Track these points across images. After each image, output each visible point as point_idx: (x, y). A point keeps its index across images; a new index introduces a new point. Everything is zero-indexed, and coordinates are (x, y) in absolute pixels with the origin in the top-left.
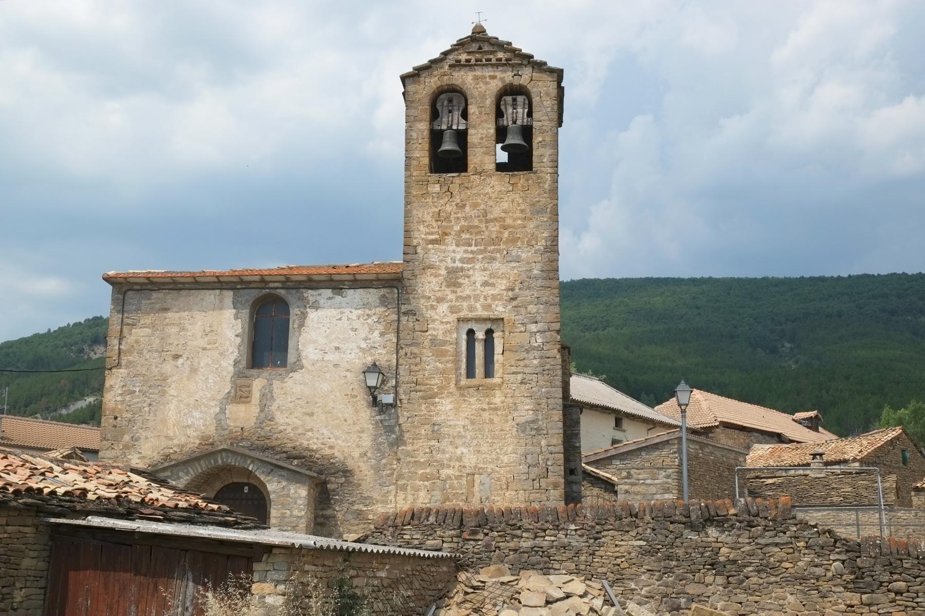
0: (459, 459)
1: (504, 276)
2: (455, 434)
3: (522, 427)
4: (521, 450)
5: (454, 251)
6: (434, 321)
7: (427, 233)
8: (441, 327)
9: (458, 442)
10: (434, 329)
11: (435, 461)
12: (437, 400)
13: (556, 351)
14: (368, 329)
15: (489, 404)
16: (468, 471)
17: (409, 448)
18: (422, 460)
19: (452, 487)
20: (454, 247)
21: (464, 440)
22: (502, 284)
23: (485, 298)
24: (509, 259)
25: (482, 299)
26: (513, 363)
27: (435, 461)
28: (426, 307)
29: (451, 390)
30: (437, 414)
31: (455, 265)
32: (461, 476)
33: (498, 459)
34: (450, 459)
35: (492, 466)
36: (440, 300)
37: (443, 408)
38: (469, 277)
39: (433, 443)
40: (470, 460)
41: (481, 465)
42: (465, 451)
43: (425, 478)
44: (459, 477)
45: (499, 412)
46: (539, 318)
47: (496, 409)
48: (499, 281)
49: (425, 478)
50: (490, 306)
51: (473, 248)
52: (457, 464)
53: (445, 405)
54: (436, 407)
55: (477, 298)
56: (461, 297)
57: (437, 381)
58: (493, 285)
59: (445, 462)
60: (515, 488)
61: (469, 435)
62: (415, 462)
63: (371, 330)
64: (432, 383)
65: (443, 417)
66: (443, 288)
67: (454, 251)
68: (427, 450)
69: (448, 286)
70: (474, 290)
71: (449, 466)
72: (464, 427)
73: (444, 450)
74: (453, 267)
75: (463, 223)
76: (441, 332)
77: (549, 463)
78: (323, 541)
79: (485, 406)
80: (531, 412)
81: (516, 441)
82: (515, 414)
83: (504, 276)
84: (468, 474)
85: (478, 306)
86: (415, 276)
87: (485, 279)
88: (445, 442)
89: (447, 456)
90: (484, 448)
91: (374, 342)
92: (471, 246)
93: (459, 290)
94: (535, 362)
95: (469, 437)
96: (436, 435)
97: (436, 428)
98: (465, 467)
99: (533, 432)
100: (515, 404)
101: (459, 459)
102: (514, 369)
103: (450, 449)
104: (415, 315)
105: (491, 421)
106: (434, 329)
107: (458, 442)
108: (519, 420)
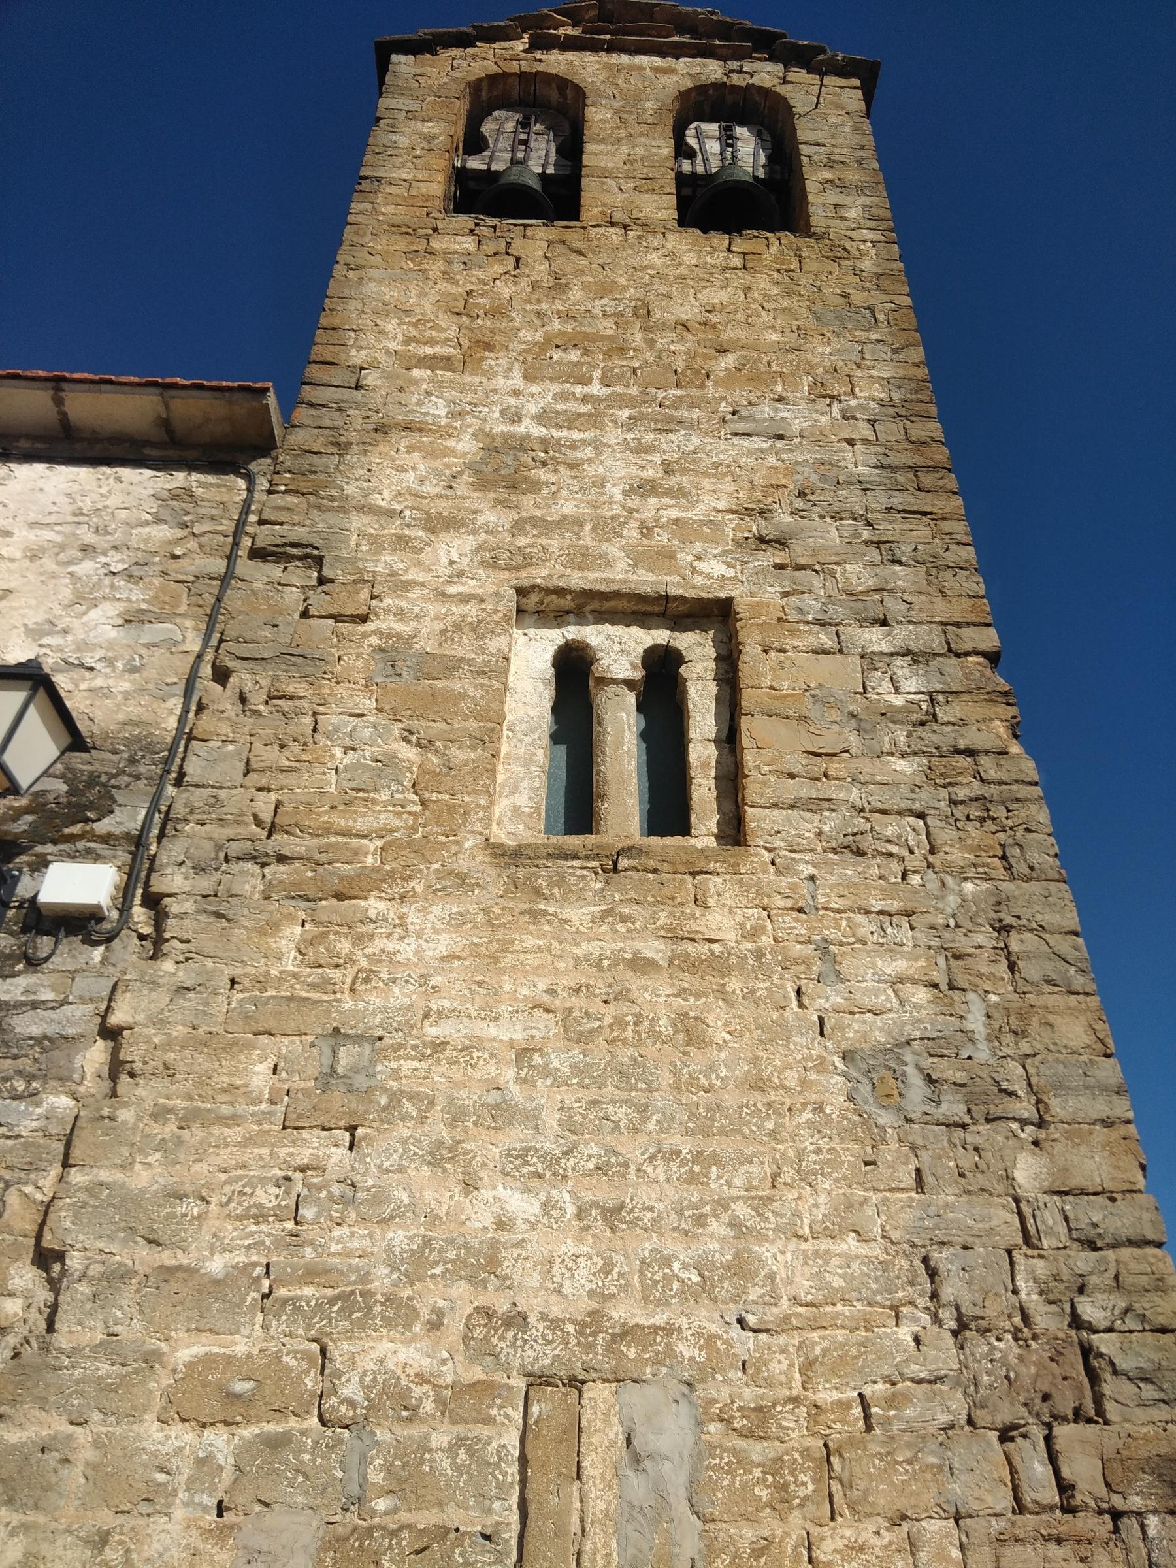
0: (483, 1264)
1: (720, 470)
2: (468, 1098)
3: (875, 1071)
4: (904, 1212)
5: (516, 393)
6: (407, 586)
7: (408, 340)
8: (435, 608)
9: (488, 1147)
10: (400, 614)
11: (311, 1274)
12: (374, 905)
13: (1001, 728)
14: (67, 593)
15: (674, 936)
16: (541, 1354)
17: (146, 1176)
18: (216, 1266)
19: (409, 1481)
20: (517, 380)
21: (515, 1137)
22: (713, 499)
23: (646, 530)
24: (742, 427)
25: (631, 532)
26: (796, 762)
27: (311, 1274)
28: (374, 540)
29: (463, 864)
30: (367, 976)
31: (521, 429)
32: (485, 1390)
33: (742, 1268)
34: (415, 1265)
35: (704, 1318)
36: (437, 525)
37: (407, 949)
38: (574, 466)
39: (312, 1145)
40: (561, 1275)
41: (620, 1312)
42: (522, 1205)
43: (212, 1399)
44: (466, 1401)
45: (734, 985)
46: (895, 607)
47: (719, 965)
48: (706, 484)
49: (212, 1399)
50: (669, 555)
51: (596, 389)
52: (461, 1297)
53: (418, 939)
54: (361, 940)
55: (607, 528)
56: (535, 522)
57: (387, 818)
58: (679, 493)
59: (382, 1280)
60: (883, 1498)
61: (549, 1101)
62: (168, 1272)
63: (84, 599)
64: (360, 824)
65: (399, 996)
66: (462, 490)
67: (516, 393)
68: (267, 1197)
69: (482, 484)
70: (596, 505)
71: (400, 1314)
72: (523, 1054)
73: (379, 1197)
74: (506, 437)
75: (557, 325)
76: (430, 627)
77: (1089, 1310)
78: (572, 632)
79: (654, 949)
80: (922, 995)
81: (849, 1154)
82: (828, 998)
83: (720, 470)
84: (538, 1380)
85: (613, 550)
86: (342, 447)
87: (649, 474)
88: (386, 1147)
89: (400, 1237)
90: (655, 1191)
91: (84, 646)
92: (586, 382)
93: (528, 500)
94: (903, 766)
95: (551, 1120)
96: (339, 1100)
97: (347, 1056)
98: (516, 1320)
99: (952, 1107)
100: (824, 948)
101: (483, 1264)
102: (802, 789)
103: (440, 1195)
104: (319, 561)
105: (691, 1031)
106: (400, 614)
107: (488, 1147)
108: (853, 1031)
